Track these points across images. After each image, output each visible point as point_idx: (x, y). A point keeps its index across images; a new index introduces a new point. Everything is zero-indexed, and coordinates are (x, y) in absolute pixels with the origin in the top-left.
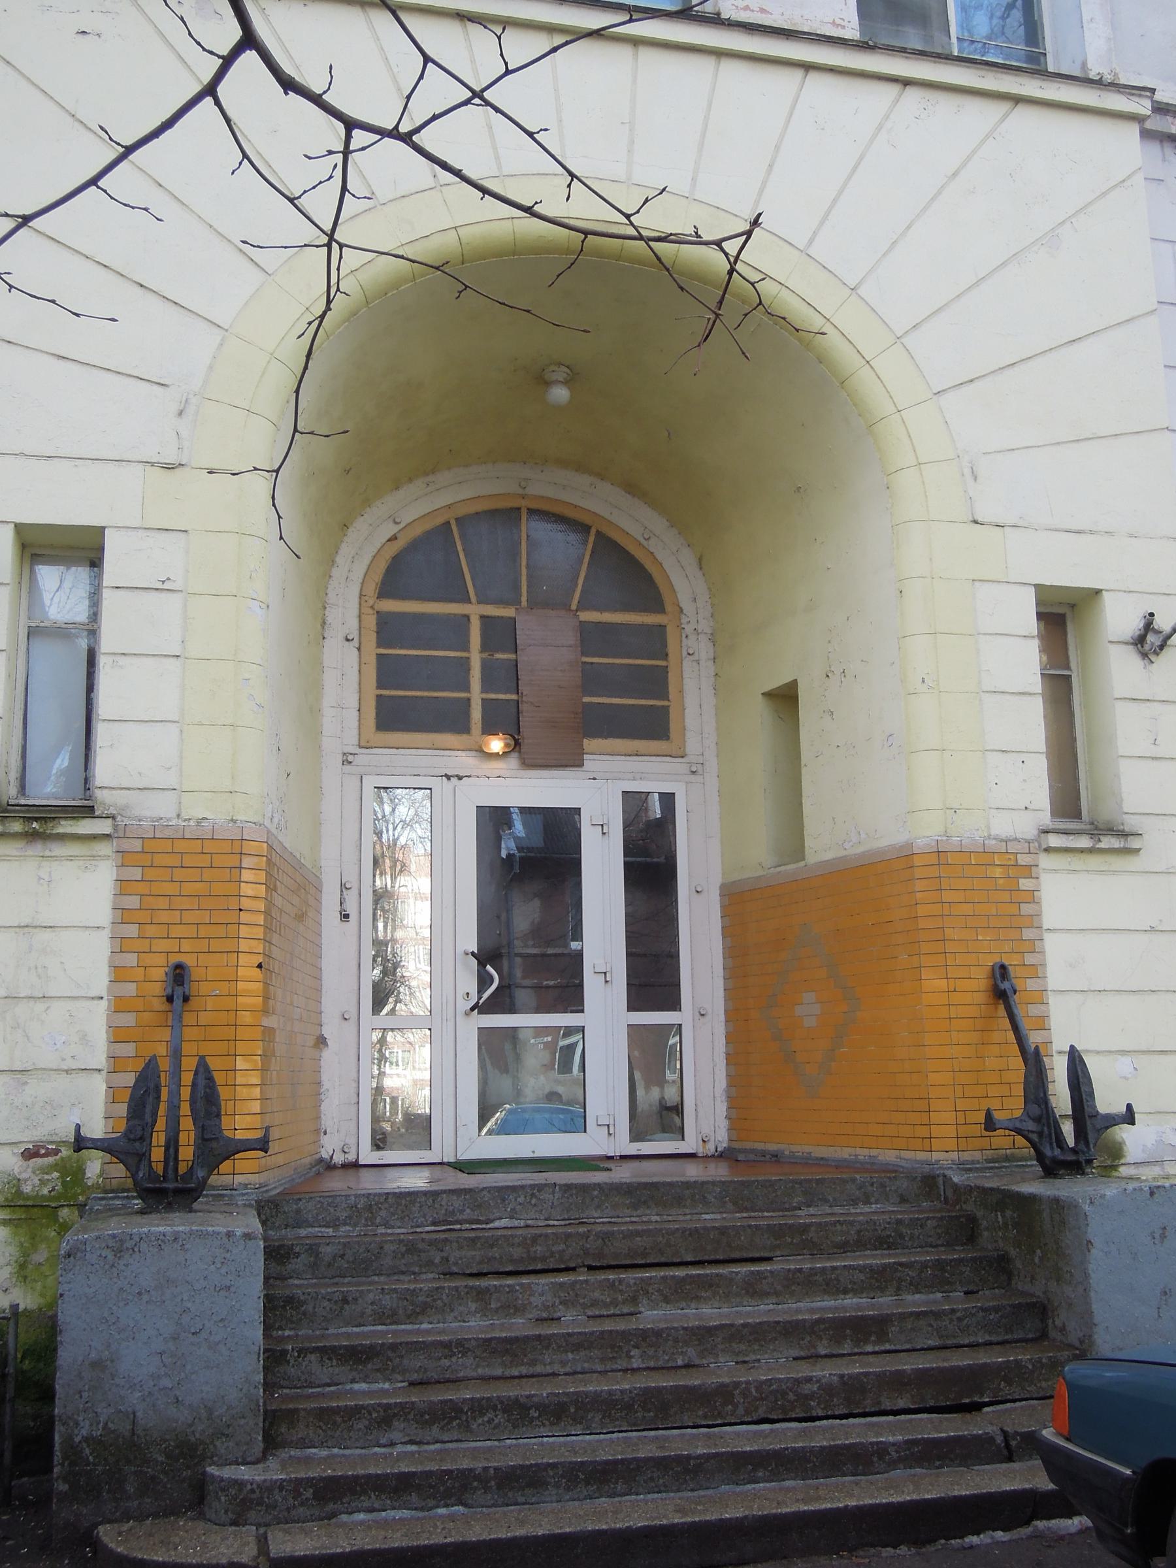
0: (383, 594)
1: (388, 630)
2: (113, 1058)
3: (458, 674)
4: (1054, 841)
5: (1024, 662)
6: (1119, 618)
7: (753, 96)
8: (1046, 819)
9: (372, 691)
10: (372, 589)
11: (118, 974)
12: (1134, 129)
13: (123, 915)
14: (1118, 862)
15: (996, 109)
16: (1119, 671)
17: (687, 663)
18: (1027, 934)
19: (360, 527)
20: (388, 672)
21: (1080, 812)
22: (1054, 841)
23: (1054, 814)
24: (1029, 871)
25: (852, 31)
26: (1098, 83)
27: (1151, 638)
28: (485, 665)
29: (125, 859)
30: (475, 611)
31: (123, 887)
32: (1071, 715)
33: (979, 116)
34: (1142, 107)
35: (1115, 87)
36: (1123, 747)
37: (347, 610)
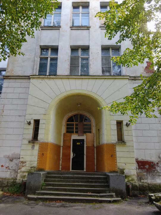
0: (67, 122)
1: (68, 125)
2: (116, 146)
3: (73, 128)
4: (117, 143)
5: (115, 127)
6: (124, 123)
7: (92, 82)
8: (117, 141)
9: (66, 130)
10: (66, 121)
11: (38, 153)
12: (128, 79)
13: (39, 149)
14: (124, 145)
15: (88, 80)
16: (125, 128)
17: (93, 127)
18: (115, 151)
19: (65, 117)
20: (67, 128)
21: (121, 139)
22: (117, 143)
23: (118, 140)
24: (115, 146)
25: (101, 75)
26: (60, 76)
27: (128, 125)
28: (75, 127)
29: (40, 144)
30: (75, 123)
31: (39, 146)
32: (122, 132)
33: (111, 81)
34: (128, 77)
35: (60, 76)
36: (125, 134)
37: (64, 123)
